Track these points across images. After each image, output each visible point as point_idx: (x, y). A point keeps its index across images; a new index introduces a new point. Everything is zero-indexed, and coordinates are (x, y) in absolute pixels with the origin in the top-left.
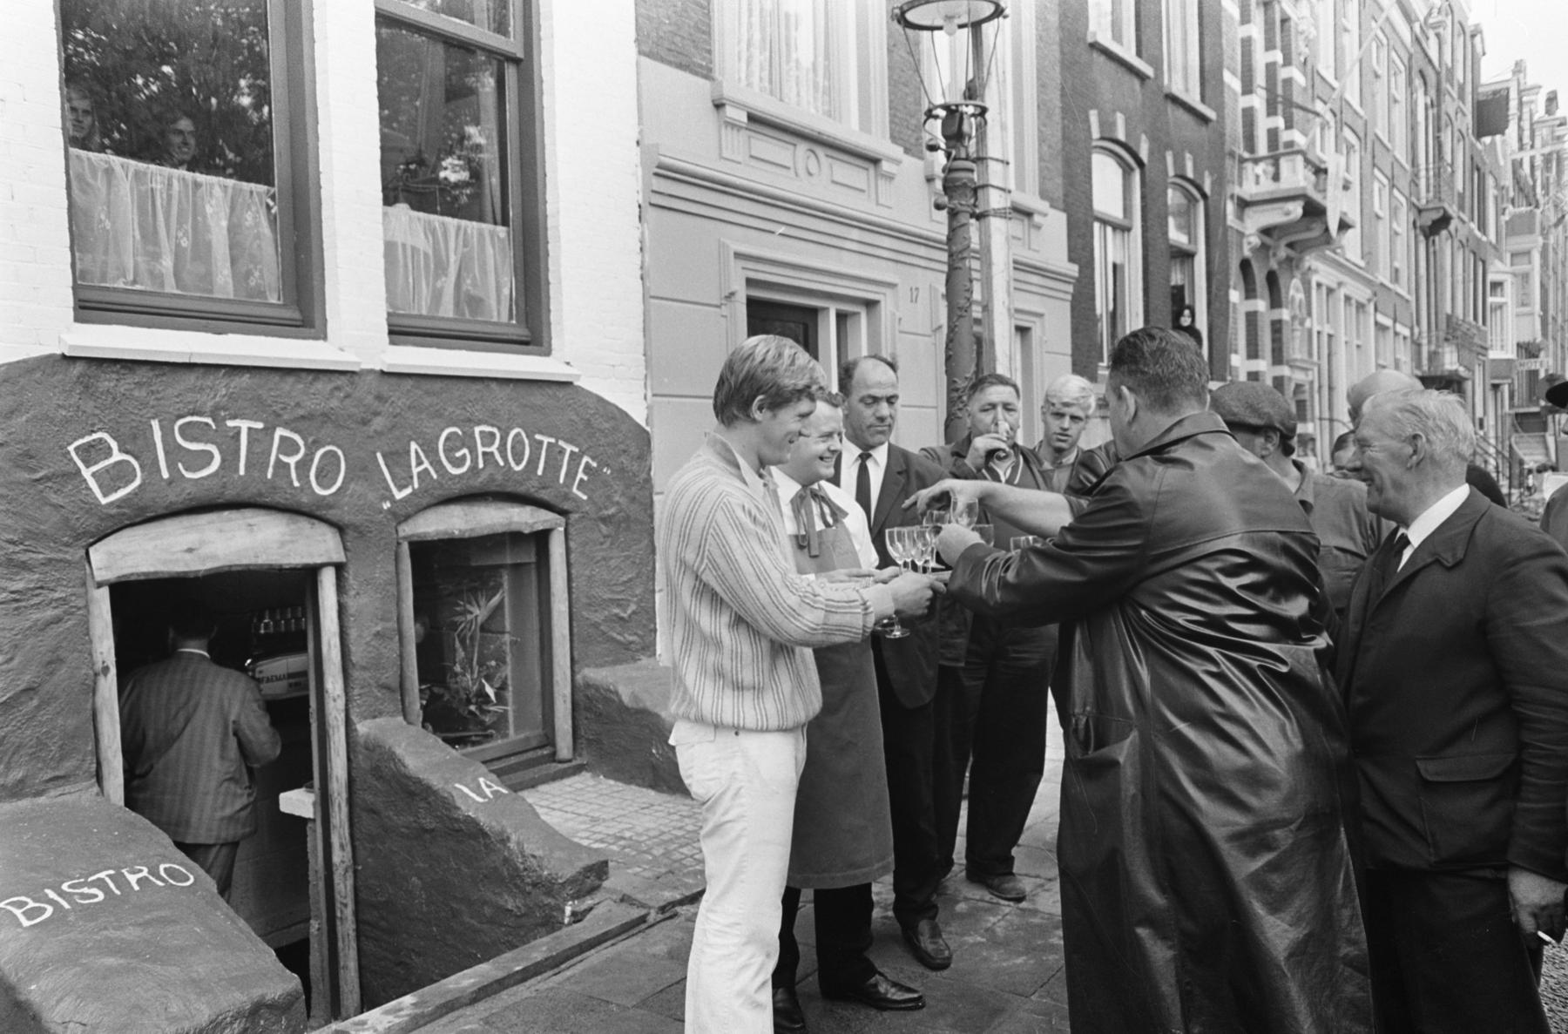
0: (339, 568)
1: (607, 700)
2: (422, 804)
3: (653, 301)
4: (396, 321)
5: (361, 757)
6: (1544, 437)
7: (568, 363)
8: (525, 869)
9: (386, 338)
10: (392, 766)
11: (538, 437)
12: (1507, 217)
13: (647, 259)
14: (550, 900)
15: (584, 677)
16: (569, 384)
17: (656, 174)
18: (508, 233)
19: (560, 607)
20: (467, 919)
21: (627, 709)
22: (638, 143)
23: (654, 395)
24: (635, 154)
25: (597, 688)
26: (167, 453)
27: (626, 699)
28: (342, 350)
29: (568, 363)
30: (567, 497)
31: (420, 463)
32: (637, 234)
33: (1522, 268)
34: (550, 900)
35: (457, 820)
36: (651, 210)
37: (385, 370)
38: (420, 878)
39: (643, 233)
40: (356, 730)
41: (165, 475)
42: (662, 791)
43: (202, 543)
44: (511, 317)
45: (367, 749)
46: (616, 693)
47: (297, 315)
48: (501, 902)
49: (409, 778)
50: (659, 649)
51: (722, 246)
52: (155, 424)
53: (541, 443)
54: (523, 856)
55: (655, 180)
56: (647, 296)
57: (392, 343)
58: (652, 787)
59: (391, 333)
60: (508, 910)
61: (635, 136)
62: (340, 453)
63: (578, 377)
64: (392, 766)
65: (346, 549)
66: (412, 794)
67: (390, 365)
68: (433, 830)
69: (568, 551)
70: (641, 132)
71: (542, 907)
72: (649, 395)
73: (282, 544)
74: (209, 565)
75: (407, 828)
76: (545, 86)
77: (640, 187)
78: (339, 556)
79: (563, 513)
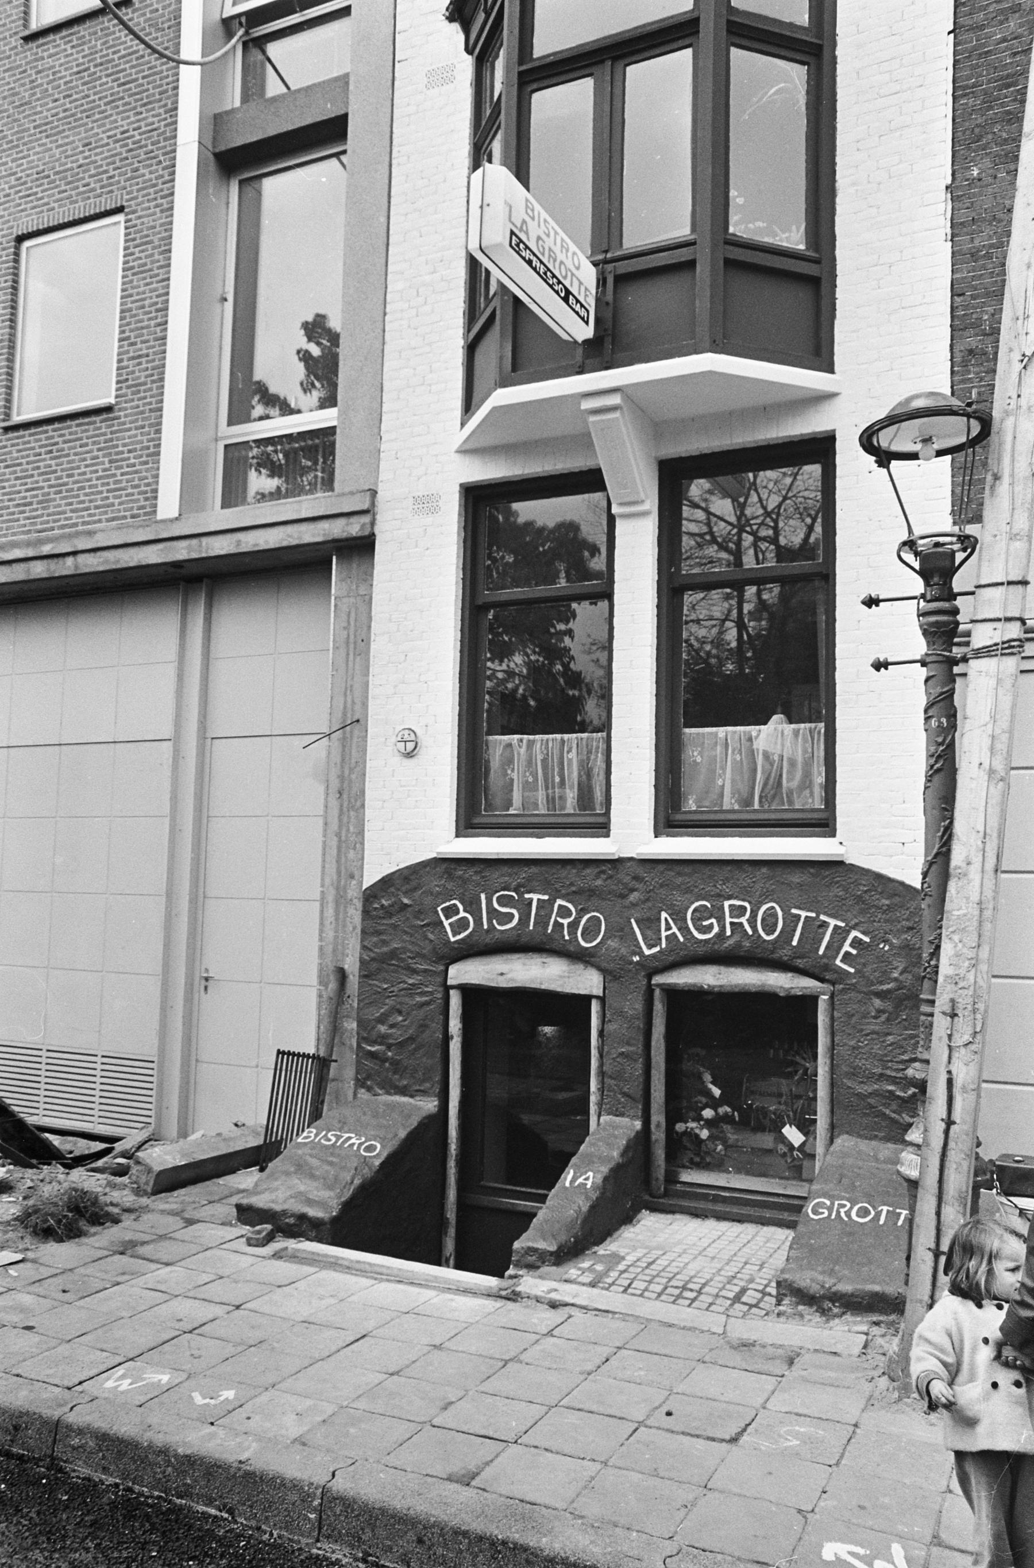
26: (488, 913)
52: (483, 896)
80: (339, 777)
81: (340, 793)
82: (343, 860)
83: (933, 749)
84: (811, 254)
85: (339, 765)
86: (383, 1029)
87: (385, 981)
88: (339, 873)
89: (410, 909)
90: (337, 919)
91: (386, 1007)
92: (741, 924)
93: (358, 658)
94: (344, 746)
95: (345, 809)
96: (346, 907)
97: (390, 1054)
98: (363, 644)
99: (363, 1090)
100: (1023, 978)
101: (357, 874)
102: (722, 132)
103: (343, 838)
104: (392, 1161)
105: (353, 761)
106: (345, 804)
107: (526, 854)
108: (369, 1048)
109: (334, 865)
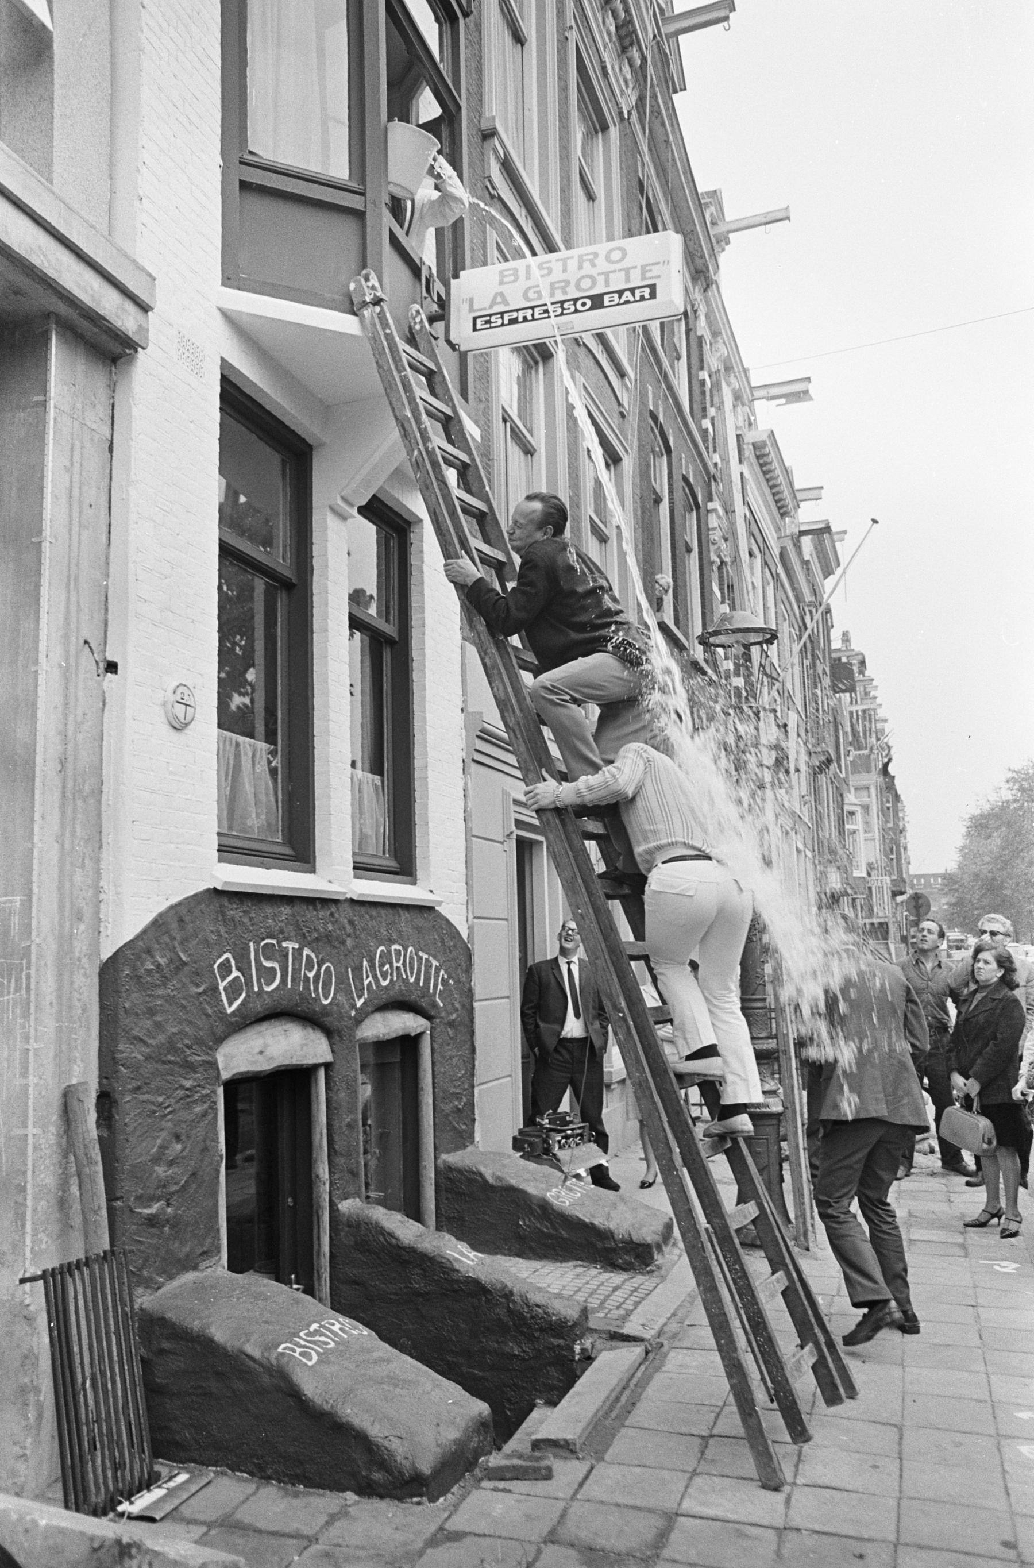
0: (327, 1066)
1: (470, 1181)
2: (417, 1271)
3: (474, 839)
4: (358, 859)
5: (342, 1234)
6: (887, 944)
7: (431, 891)
8: (532, 1317)
9: (352, 872)
10: (382, 1239)
11: (421, 953)
12: (851, 758)
13: (470, 804)
14: (561, 1342)
15: (444, 1162)
16: (430, 909)
17: (478, 737)
18: (383, 782)
19: (427, 1100)
20: (465, 1370)
21: (492, 1187)
22: (462, 710)
23: (475, 918)
24: (459, 719)
25: (460, 1171)
26: (257, 970)
27: (491, 1180)
28: (330, 882)
29: (431, 891)
30: (434, 1005)
31: (368, 977)
32: (461, 784)
33: (866, 800)
34: (561, 1342)
35: (458, 1281)
36: (474, 765)
37: (219, 888)
38: (409, 1339)
39: (466, 784)
40: (338, 1210)
41: (256, 989)
42: (529, 1258)
43: (266, 1046)
44: (384, 853)
45: (349, 1226)
46: (480, 1174)
47: (291, 852)
48: (507, 1349)
49: (404, 1248)
50: (477, 1137)
51: (506, 794)
52: (251, 944)
53: (287, 948)
54: (528, 1306)
55: (478, 742)
56: (469, 835)
57: (356, 877)
58: (520, 1255)
59: (355, 868)
60: (515, 1355)
61: (460, 705)
62: (216, 966)
63: (440, 903)
64: (382, 1239)
65: (333, 1051)
66: (405, 1263)
67: (360, 895)
68: (427, 1293)
69: (432, 1049)
70: (464, 702)
71: (552, 1348)
72: (471, 916)
73: (302, 1046)
74: (274, 1065)
75: (396, 1294)
76: (415, 664)
77: (463, 745)
78: (329, 1058)
79: (429, 1017)
80: (60, 733)
81: (61, 762)
82: (67, 885)
83: (766, 939)
84: (354, 185)
85: (60, 709)
86: (160, 1170)
87: (159, 1091)
88: (61, 908)
89: (186, 968)
90: (59, 997)
91: (164, 1134)
92: (231, 972)
93: (85, 534)
94: (67, 680)
95: (69, 794)
96: (72, 972)
97: (169, 1210)
98: (91, 512)
99: (140, 1290)
100: (495, 999)
101: (88, 913)
102: (382, 140)
103: (67, 846)
104: (602, 1071)
105: (80, 711)
106: (70, 784)
107: (415, 899)
108: (147, 1211)
109: (55, 894)
